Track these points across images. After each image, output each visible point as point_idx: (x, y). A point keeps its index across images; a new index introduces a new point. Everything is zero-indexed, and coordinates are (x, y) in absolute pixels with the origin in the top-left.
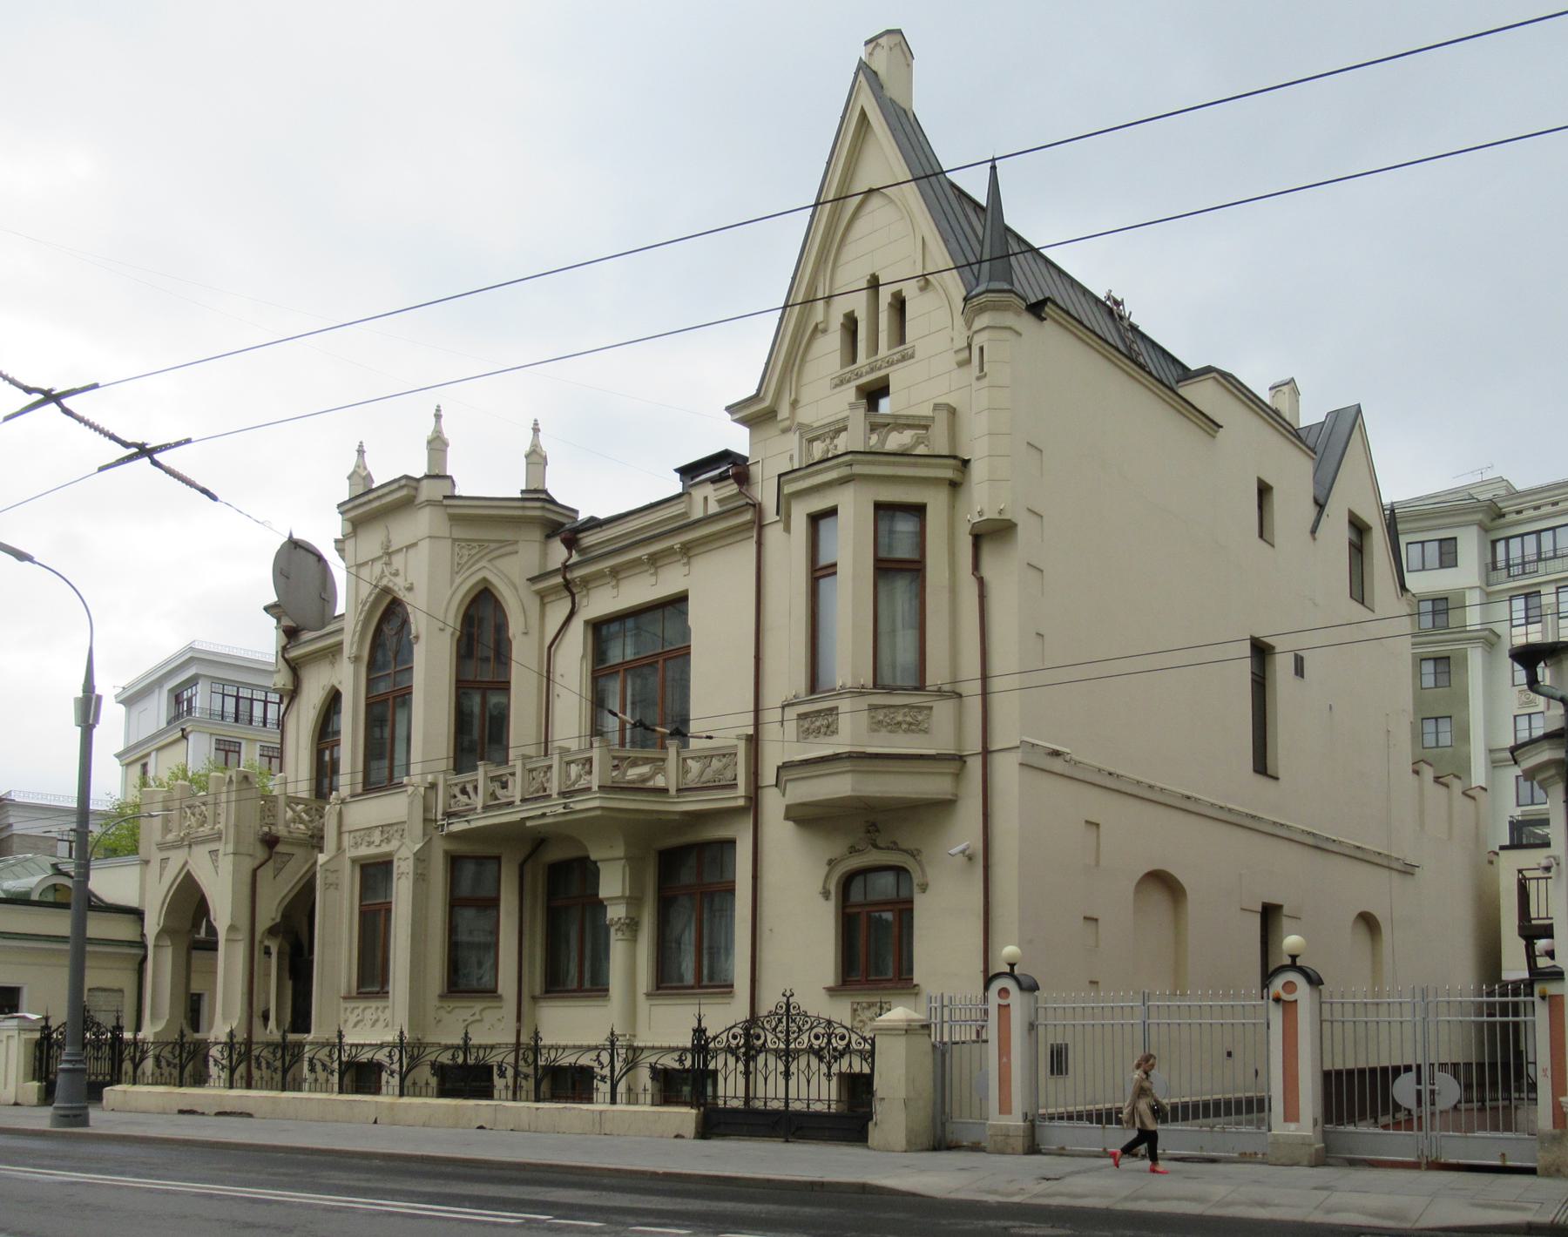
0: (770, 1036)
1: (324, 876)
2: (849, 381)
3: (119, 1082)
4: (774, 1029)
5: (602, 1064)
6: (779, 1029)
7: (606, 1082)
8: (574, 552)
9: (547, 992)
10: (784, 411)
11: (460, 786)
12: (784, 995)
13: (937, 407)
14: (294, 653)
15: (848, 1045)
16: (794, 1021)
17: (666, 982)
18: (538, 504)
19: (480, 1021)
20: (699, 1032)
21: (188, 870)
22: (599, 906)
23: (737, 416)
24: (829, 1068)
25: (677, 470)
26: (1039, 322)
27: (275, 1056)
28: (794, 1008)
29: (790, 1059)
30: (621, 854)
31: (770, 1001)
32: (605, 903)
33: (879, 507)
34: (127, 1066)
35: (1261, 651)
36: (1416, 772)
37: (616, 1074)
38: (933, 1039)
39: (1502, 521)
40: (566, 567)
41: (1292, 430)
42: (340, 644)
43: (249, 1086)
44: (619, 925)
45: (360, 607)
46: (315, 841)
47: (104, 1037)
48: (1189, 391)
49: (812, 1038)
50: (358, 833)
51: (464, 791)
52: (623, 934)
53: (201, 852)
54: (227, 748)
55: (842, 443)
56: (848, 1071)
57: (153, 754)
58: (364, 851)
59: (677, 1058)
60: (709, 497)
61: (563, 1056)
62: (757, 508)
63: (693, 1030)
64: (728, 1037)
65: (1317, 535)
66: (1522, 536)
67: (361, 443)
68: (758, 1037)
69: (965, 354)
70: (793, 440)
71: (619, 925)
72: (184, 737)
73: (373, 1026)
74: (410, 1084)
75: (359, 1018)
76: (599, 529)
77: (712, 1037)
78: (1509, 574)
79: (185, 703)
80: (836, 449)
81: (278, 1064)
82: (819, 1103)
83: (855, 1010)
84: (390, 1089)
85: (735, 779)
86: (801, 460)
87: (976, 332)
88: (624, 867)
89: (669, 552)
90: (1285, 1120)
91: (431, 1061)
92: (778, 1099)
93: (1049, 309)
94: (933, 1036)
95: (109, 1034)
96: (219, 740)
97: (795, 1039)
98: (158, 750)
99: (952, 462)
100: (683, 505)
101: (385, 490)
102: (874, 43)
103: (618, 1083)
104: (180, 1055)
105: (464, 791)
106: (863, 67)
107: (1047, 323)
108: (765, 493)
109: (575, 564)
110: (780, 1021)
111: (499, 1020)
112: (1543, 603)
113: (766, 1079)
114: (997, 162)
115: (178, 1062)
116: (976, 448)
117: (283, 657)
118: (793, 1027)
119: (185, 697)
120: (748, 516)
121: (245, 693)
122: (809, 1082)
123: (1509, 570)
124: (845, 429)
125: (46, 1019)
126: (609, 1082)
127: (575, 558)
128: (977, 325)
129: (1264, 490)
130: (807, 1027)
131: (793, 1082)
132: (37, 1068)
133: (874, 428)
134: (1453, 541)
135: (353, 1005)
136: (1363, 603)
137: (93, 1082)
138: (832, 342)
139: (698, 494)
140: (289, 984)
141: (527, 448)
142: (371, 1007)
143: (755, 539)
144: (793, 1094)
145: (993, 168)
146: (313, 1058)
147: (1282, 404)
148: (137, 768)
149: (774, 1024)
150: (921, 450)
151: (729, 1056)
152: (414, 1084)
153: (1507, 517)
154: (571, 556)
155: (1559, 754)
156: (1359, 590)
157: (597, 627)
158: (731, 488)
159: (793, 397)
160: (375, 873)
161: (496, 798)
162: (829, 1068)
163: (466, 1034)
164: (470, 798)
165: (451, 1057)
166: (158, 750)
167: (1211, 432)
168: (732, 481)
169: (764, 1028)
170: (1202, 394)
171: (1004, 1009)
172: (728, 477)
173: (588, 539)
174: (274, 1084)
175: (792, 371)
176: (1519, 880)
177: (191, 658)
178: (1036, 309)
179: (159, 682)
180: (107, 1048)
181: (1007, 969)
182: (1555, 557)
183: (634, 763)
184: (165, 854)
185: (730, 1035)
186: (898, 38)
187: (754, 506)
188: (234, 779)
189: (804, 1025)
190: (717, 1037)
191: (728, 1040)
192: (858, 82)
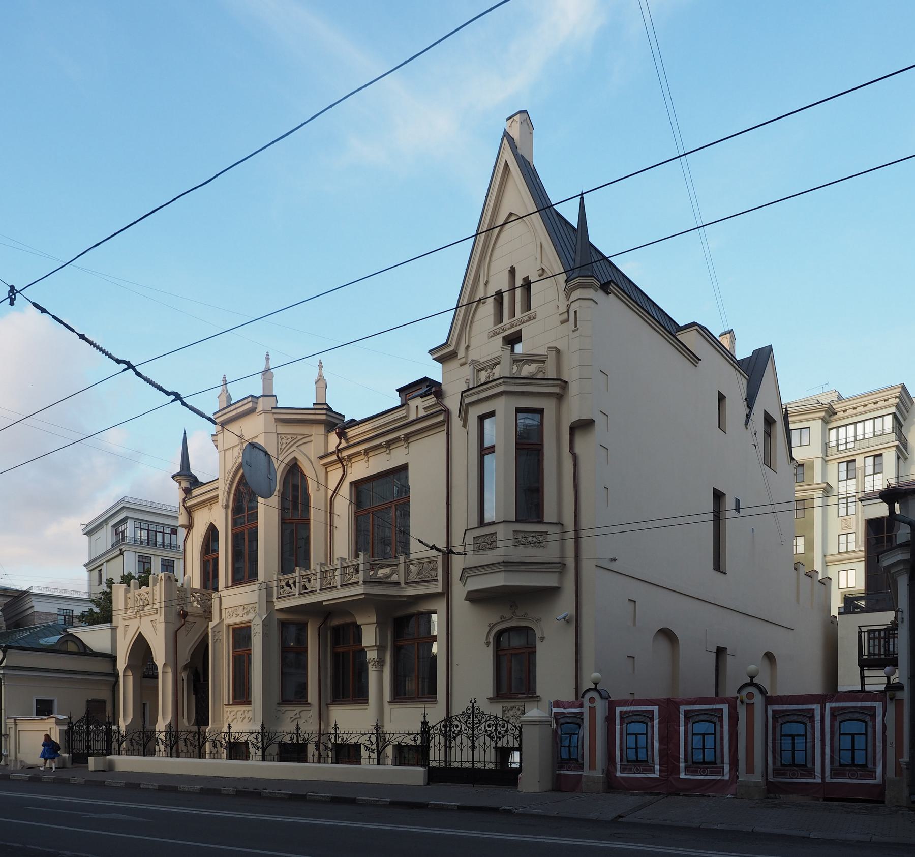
0: (463, 726)
1: (213, 635)
2: (498, 334)
3: (111, 754)
4: (466, 722)
5: (372, 742)
6: (469, 722)
7: (374, 753)
8: (342, 440)
9: (334, 701)
10: (461, 353)
11: (286, 581)
12: (471, 702)
13: (550, 349)
14: (189, 503)
15: (507, 731)
16: (476, 717)
17: (400, 694)
18: (324, 412)
19: (300, 717)
20: (425, 723)
21: (140, 632)
22: (363, 651)
23: (435, 356)
24: (496, 744)
25: (397, 390)
26: (607, 295)
27: (194, 739)
28: (477, 709)
29: (475, 739)
30: (375, 621)
31: (459, 708)
32: (366, 649)
33: (519, 410)
34: (115, 745)
35: (718, 496)
36: (796, 569)
37: (380, 748)
38: (552, 727)
39: (836, 417)
40: (339, 450)
41: (735, 360)
42: (217, 497)
43: (178, 756)
44: (373, 662)
45: (227, 475)
46: (207, 614)
47: (101, 728)
48: (682, 337)
49: (487, 727)
50: (230, 610)
51: (288, 585)
52: (376, 668)
53: (146, 621)
54: (144, 560)
55: (497, 372)
56: (507, 746)
57: (105, 564)
58: (234, 620)
59: (413, 739)
60: (419, 405)
61: (210, 736)
62: (447, 412)
63: (421, 722)
64: (440, 727)
65: (748, 426)
66: (846, 425)
67: (225, 376)
68: (457, 727)
69: (566, 316)
70: (468, 371)
71: (373, 662)
72: (122, 554)
73: (242, 721)
74: (268, 754)
75: (235, 717)
76: (357, 427)
77: (431, 726)
78: (838, 449)
79: (121, 534)
80: (493, 376)
81: (197, 743)
82: (491, 764)
83: (504, 711)
84: (257, 757)
85: (436, 576)
86: (474, 384)
87: (572, 302)
88: (376, 628)
89: (397, 439)
90: (746, 773)
91: (398, 742)
92: (480, 762)
93: (612, 287)
94: (552, 726)
95: (104, 727)
96: (140, 556)
97: (478, 727)
98: (107, 561)
99: (559, 382)
100: (405, 411)
101: (240, 404)
102: (512, 119)
103: (265, 750)
104: (143, 738)
105: (288, 585)
106: (506, 135)
107: (611, 295)
108: (452, 403)
109: (345, 448)
110: (469, 717)
111: (309, 717)
112: (856, 467)
113: (461, 751)
114: (584, 195)
115: (261, 746)
116: (570, 374)
117: (184, 506)
118: (476, 720)
119: (120, 530)
120: (441, 418)
121: (152, 528)
122: (439, 751)
123: (838, 447)
124: (499, 363)
125: (70, 718)
126: (376, 752)
127: (344, 444)
128: (572, 299)
129: (721, 398)
130: (484, 720)
131: (476, 752)
132: (67, 746)
133: (515, 361)
134: (808, 429)
135: (231, 709)
136: (770, 467)
137: (82, 753)
138: (488, 308)
139: (413, 404)
140: (193, 697)
141: (316, 378)
142: (241, 710)
143: (446, 431)
144: (476, 759)
145: (582, 199)
146: (215, 740)
147: (725, 342)
148: (96, 572)
149: (465, 719)
150: (540, 376)
151: (441, 737)
152: (149, 750)
153: (838, 414)
154: (340, 443)
155: (907, 556)
156: (769, 461)
157: (355, 485)
158: (431, 400)
159: (467, 344)
160: (241, 635)
161: (307, 589)
162: (496, 744)
163: (298, 725)
164: (291, 589)
165: (290, 739)
166: (107, 561)
167: (696, 364)
168: (433, 396)
169: (460, 721)
170: (690, 339)
171: (592, 710)
172: (430, 394)
173: (351, 433)
174: (195, 754)
175: (466, 328)
176: (859, 632)
177: (123, 507)
178: (605, 288)
179: (106, 521)
180: (103, 734)
181: (593, 686)
182: (883, 434)
183: (382, 567)
184: (127, 623)
185: (487, 725)
186: (525, 116)
187: (445, 411)
188: (163, 578)
189: (482, 719)
190: (435, 726)
191: (485, 728)
192: (503, 144)
